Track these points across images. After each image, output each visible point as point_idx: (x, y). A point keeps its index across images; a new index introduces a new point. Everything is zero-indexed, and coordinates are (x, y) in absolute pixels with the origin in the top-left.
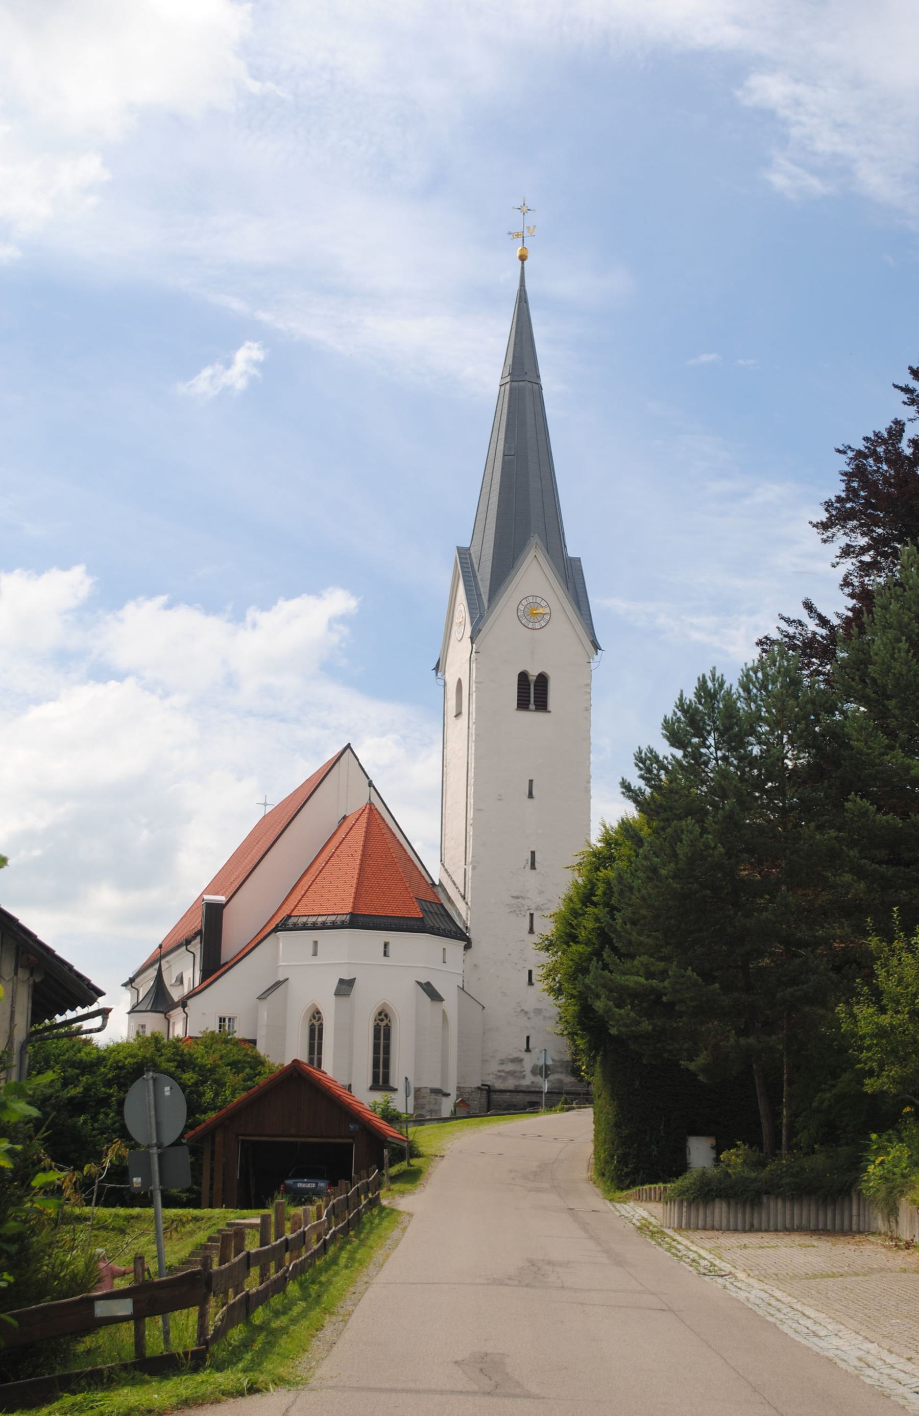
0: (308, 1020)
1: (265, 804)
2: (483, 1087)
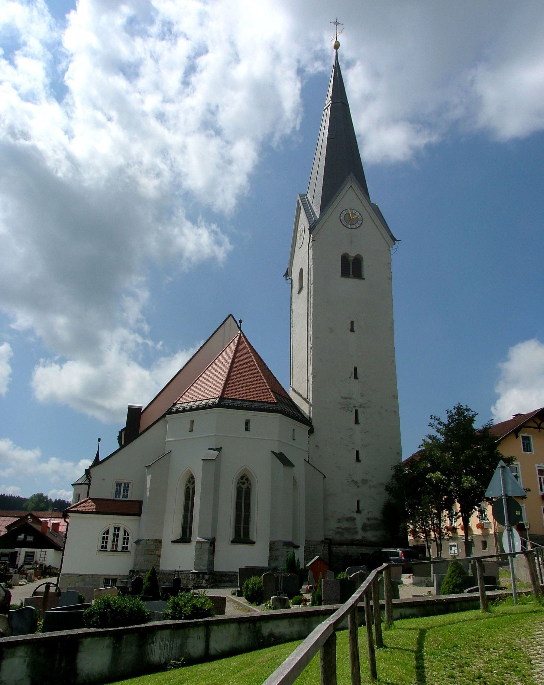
0: (185, 484)
2: (326, 541)
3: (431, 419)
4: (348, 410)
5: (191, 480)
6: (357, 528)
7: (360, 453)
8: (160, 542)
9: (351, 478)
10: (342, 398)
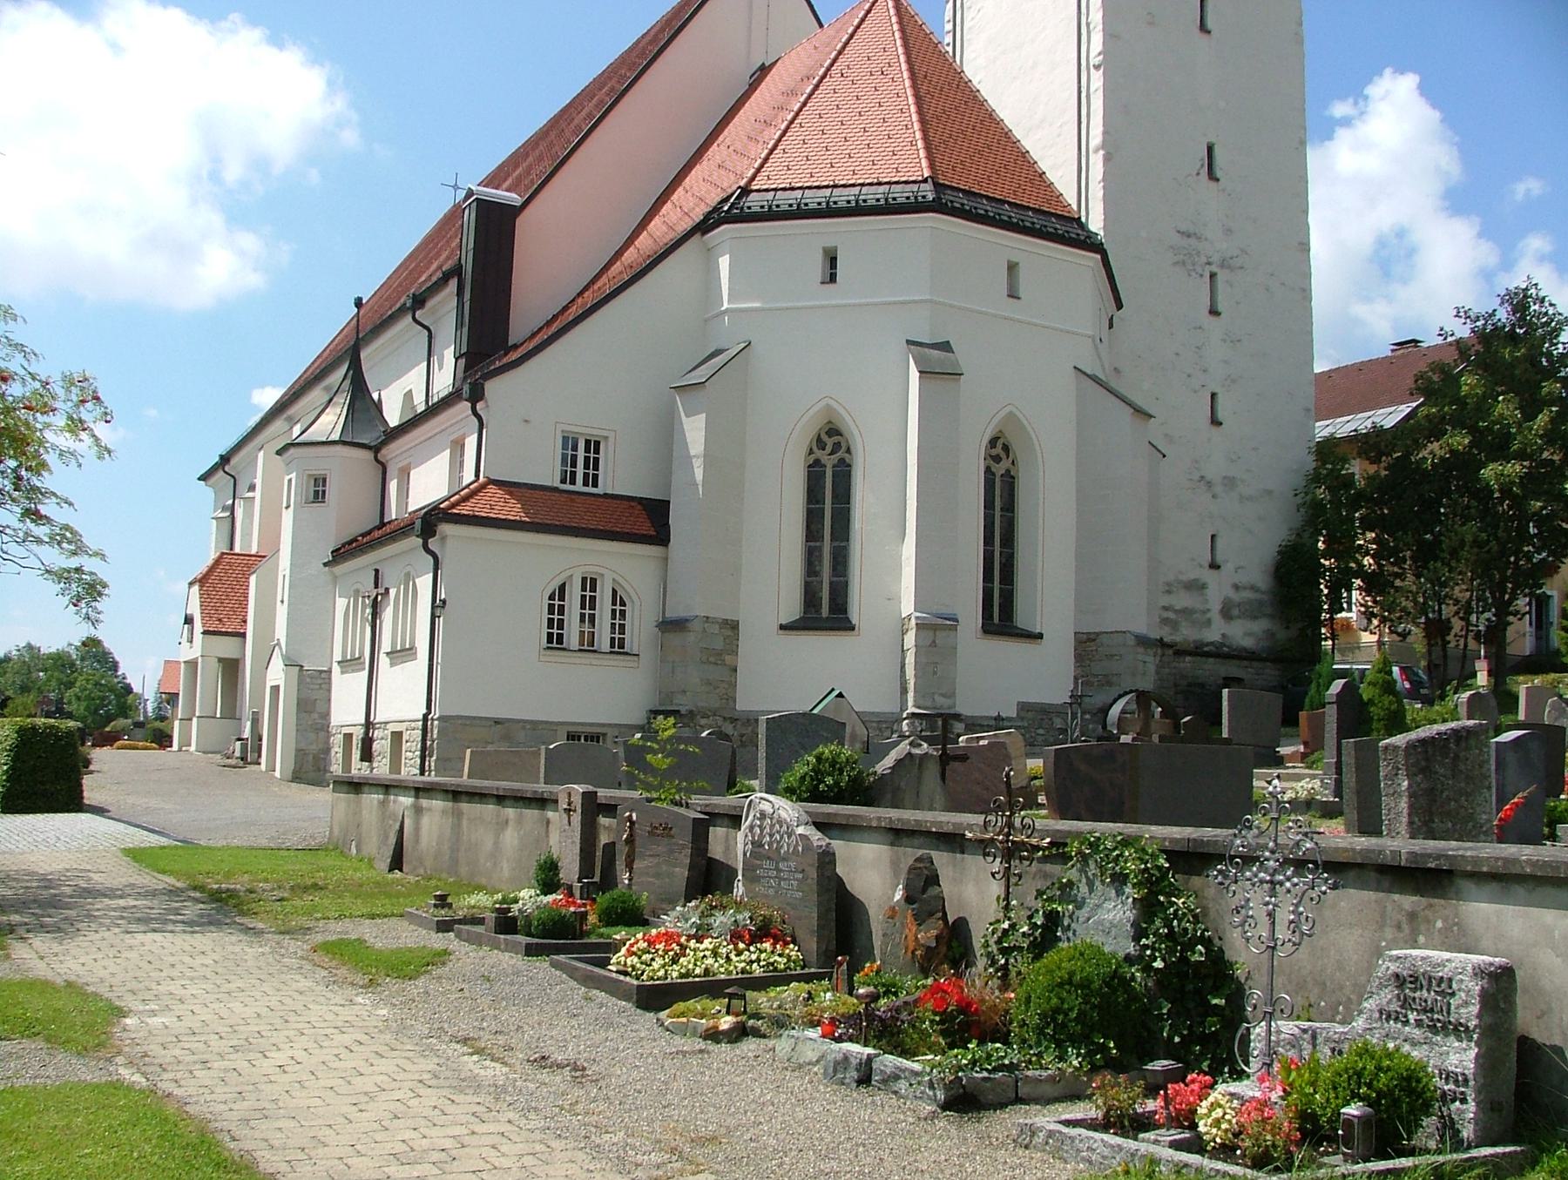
0: (804, 450)
1: (456, 187)
3: (1456, 316)
4: (1194, 270)
5: (825, 437)
6: (1209, 610)
7: (1220, 399)
8: (734, 626)
10: (1179, 232)
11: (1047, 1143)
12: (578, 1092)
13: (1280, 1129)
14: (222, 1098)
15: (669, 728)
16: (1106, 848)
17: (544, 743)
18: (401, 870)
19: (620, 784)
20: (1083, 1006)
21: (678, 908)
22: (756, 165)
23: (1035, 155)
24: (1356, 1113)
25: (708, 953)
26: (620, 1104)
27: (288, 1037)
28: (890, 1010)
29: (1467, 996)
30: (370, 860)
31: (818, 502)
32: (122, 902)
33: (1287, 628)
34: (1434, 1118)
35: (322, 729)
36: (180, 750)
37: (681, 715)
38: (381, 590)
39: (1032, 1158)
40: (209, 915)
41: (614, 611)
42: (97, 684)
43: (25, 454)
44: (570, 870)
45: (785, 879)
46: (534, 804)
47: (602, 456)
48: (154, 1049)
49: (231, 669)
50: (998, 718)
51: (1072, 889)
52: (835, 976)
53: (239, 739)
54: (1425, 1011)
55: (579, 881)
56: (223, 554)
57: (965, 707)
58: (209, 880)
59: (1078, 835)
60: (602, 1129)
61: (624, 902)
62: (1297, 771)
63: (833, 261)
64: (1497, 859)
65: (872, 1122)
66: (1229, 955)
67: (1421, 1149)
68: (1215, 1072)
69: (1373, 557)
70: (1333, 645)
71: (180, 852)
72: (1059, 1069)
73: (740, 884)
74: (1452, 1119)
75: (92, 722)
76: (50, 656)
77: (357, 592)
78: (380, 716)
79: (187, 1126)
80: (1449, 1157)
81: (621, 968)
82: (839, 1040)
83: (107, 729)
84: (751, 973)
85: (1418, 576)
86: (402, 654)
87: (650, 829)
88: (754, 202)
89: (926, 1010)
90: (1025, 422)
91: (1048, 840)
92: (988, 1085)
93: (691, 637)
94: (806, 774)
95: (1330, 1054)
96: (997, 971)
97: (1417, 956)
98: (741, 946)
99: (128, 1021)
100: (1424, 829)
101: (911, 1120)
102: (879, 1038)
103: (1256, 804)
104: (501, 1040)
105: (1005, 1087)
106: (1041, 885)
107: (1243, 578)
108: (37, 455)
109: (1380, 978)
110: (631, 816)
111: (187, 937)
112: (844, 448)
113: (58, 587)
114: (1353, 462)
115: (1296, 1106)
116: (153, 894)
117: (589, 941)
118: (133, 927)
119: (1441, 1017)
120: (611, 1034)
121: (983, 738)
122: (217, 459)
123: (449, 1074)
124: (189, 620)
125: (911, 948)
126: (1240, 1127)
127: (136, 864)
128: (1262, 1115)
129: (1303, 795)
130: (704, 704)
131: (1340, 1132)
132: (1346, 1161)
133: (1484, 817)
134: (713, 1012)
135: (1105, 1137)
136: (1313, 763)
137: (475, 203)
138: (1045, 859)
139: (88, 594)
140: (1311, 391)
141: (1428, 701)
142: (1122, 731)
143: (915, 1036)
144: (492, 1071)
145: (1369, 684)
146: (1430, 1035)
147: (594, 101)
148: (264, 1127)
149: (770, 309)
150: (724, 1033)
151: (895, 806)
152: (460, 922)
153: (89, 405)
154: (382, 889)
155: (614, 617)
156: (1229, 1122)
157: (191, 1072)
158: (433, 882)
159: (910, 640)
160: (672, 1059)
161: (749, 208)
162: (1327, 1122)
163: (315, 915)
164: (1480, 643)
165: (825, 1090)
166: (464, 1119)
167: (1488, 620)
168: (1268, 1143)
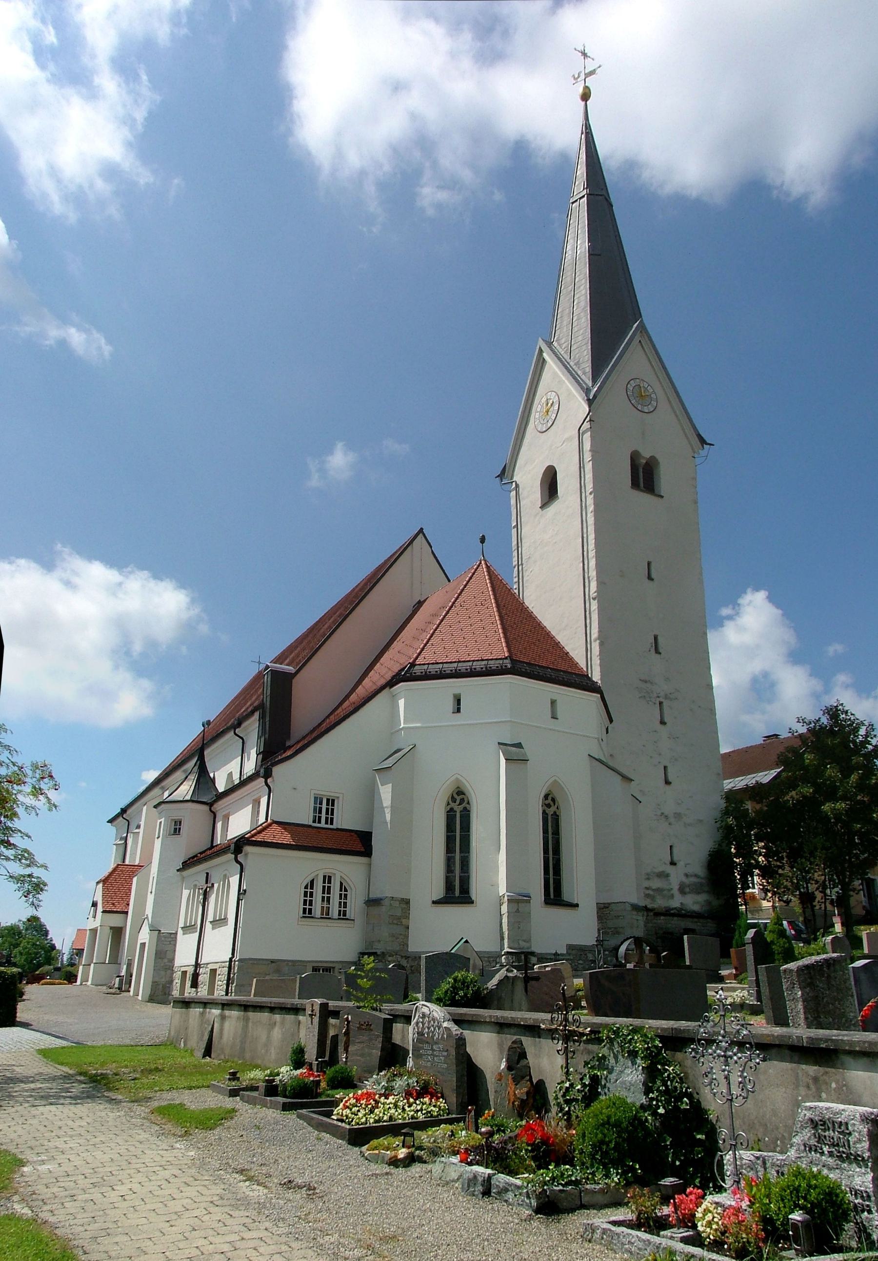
1: (259, 663)
5: (455, 796)
7: (669, 770)
8: (407, 902)
9: (660, 809)
11: (602, 1238)
12: (311, 1206)
13: (751, 1229)
14: (80, 1222)
15: (371, 963)
16: (623, 1034)
17: (299, 974)
18: (210, 1057)
19: (342, 998)
20: (618, 1139)
21: (374, 1076)
22: (418, 652)
23: (563, 643)
24: (799, 1218)
25: (391, 1106)
26: (336, 1214)
27: (129, 1175)
28: (501, 1143)
29: (859, 1135)
30: (192, 1051)
31: (452, 832)
32: (32, 1086)
33: (718, 899)
34: (852, 1224)
35: (169, 969)
36: (81, 984)
37: (378, 955)
38: (209, 885)
39: (594, 1249)
40: (88, 1092)
41: (341, 895)
42: (34, 944)
43: (4, 808)
44: (311, 1054)
45: (437, 1056)
46: (291, 1012)
47: (335, 808)
48: (40, 1188)
49: (117, 933)
50: (556, 954)
51: (605, 1061)
52: (467, 1120)
53: (118, 977)
54: (833, 1145)
55: (317, 1060)
56: (118, 865)
57: (537, 948)
58: (90, 1068)
59: (606, 1026)
60: (324, 1233)
61: (342, 1073)
62: (732, 985)
63: (459, 702)
64: (865, 1042)
65: (492, 1223)
66: (704, 1105)
67: (846, 1247)
68: (704, 1187)
69: (764, 856)
70: (746, 908)
71: (74, 1050)
72: (606, 1184)
73: (411, 1059)
74: (864, 1226)
75: (28, 968)
76: (6, 928)
77: (195, 886)
78: (204, 960)
79: (55, 1245)
80: (867, 1254)
81: (339, 1117)
82: (470, 1164)
83: (37, 973)
84: (417, 1119)
85: (792, 867)
86: (220, 922)
87: (358, 1025)
88: (417, 670)
89: (522, 1142)
90: (563, 786)
91: (589, 1029)
92: (563, 1195)
93: (384, 909)
94: (448, 989)
95: (776, 1175)
96: (564, 1115)
97: (823, 1107)
98: (411, 1100)
99: (25, 1169)
100: (815, 1022)
101: (517, 1221)
102: (495, 1162)
103: (710, 1006)
104: (264, 1170)
105: (573, 1197)
106: (587, 1058)
107: (690, 870)
108: (12, 808)
109: (801, 1122)
110: (348, 1018)
111: (72, 1107)
112: (466, 802)
113: (16, 886)
114: (746, 802)
115: (759, 1212)
116: (54, 1079)
117: (321, 1099)
118: (37, 1102)
119: (844, 1150)
120: (332, 1164)
121: (548, 966)
122: (119, 810)
123: (230, 1196)
124: (94, 904)
125: (512, 1100)
126: (724, 1227)
127: (45, 1060)
128: (738, 1219)
129: (738, 1000)
130: (391, 948)
131: (791, 1233)
132: (797, 1255)
133: (852, 1014)
134: (394, 1145)
135: (639, 1234)
136: (742, 980)
137: (270, 673)
138: (588, 1042)
139: (34, 890)
140: (720, 764)
141: (807, 942)
142: (628, 962)
143: (517, 1161)
144: (257, 1192)
145: (770, 931)
146: (840, 1163)
147: (332, 619)
148: (106, 1242)
149: (426, 727)
150: (400, 1160)
151: (499, 1008)
152: (244, 1089)
153: (46, 780)
154: (198, 1069)
155: (341, 898)
156: (717, 1223)
157: (63, 1204)
158: (229, 1064)
159: (504, 908)
160: (369, 1180)
161: (415, 673)
162: (781, 1225)
163: (155, 1089)
164: (834, 906)
165: (463, 1200)
166: (237, 1228)
167: (837, 892)
168: (744, 1240)
